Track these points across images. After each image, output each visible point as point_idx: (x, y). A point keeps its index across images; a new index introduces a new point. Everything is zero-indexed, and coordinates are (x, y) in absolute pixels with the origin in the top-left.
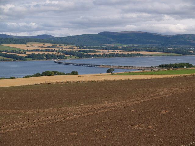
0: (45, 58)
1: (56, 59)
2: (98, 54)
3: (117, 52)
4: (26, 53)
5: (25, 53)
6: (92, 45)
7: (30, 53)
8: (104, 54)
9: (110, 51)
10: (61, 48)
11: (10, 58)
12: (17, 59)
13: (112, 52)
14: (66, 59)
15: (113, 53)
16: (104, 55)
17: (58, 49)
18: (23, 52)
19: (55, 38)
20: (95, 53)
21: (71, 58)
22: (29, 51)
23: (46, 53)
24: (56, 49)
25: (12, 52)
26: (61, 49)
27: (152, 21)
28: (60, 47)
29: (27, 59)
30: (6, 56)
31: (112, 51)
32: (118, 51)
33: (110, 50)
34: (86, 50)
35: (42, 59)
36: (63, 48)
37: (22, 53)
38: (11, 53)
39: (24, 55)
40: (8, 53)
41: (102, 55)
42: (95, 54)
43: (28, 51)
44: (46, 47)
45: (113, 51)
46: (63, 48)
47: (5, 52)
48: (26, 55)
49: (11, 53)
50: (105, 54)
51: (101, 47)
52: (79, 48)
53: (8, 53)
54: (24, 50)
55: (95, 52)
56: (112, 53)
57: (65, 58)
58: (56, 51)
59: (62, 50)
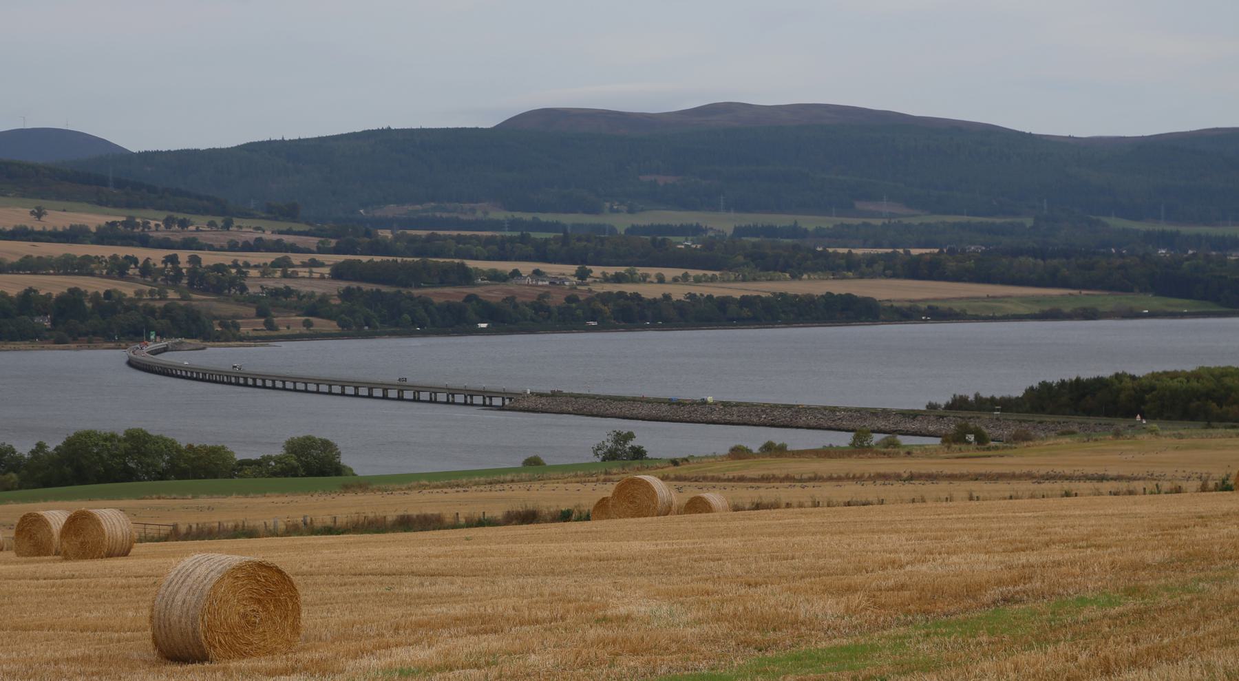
9: (597, 271)
31: (611, 271)
51: (524, 239)
52: (333, 242)
56: (615, 288)
58: (146, 270)
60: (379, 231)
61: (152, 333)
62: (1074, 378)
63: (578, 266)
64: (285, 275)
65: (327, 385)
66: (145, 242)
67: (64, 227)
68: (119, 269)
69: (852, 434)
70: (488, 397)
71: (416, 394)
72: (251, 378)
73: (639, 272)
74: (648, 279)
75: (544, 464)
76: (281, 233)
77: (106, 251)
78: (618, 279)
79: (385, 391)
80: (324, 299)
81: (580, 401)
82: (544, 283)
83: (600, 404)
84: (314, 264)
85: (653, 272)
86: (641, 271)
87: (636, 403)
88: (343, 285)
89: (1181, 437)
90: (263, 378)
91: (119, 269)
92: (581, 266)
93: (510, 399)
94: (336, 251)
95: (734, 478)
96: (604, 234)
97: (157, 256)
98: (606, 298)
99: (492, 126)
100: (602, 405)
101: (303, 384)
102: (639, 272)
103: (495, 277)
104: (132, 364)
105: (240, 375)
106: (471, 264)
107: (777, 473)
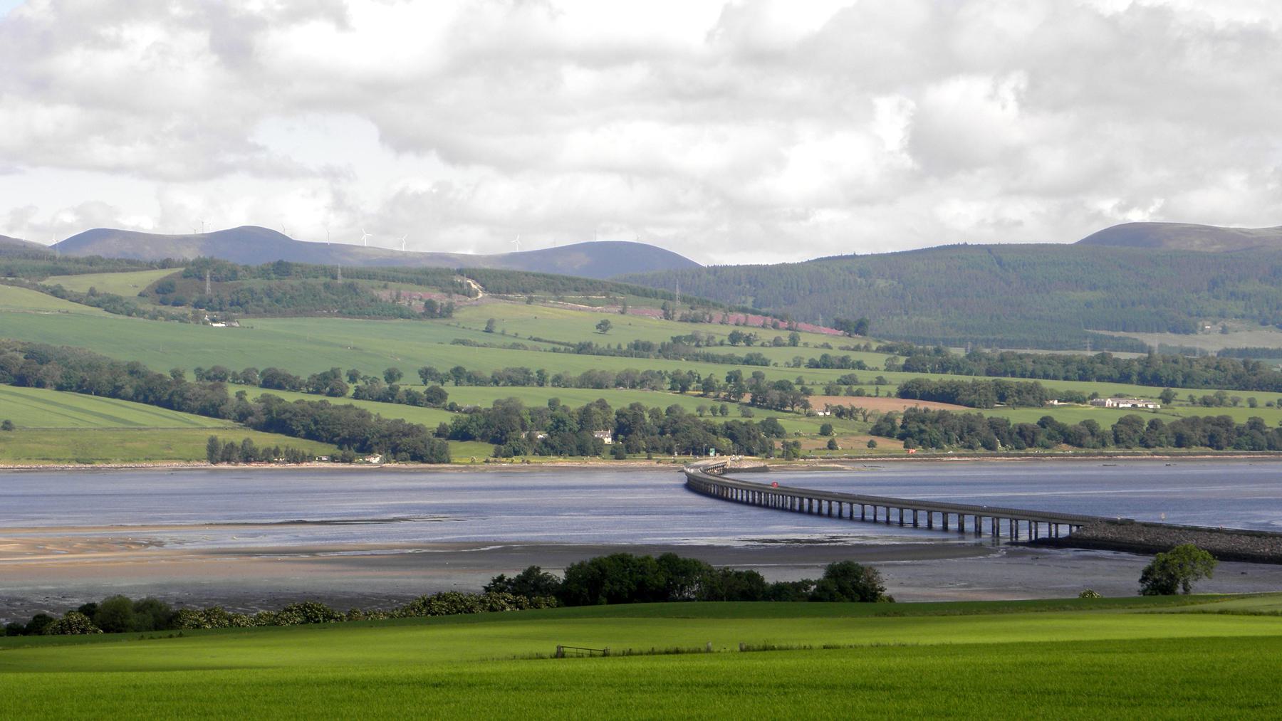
0: (608, 440)
1: (698, 450)
2: (1070, 416)
3: (1253, 404)
4: (443, 396)
5: (435, 399)
6: (1024, 344)
7: (482, 398)
8: (1256, 424)
9: (1182, 393)
10: (747, 362)
11: (310, 435)
12: (365, 448)
13: (1206, 402)
14: (791, 452)
15: (1214, 412)
16: (282, 561)
17: (720, 373)
18: (421, 389)
19: (700, 268)
20: (1044, 412)
21: (831, 446)
22: (475, 380)
23: (619, 399)
24: (704, 370)
25: (326, 383)
26: (747, 372)
27: (904, 615)
28: (741, 351)
29: (455, 447)
30: (276, 423)
31: (1199, 394)
32: (1262, 397)
33: (1184, 385)
34: (968, 379)
35: (583, 451)
36: (765, 363)
37: (413, 400)
38: (318, 392)
39: (431, 419)
40: (289, 397)
41: (1106, 425)
42: (1044, 422)
43: (459, 375)
44: (619, 352)
45: (1210, 393)
46: (765, 363)
47: (266, 384)
48: (447, 418)
49: (316, 398)
50: (1139, 422)
51: (1103, 359)
52: (902, 360)
53: (289, 397)
54: (426, 374)
55: (1041, 399)
56: (1203, 412)
57: (778, 444)
58: (708, 387)
59: (757, 376)
60: (951, 348)
61: (711, 449)
62: (1244, 347)
63: (1163, 388)
64: (850, 393)
65: (898, 508)
66: (708, 359)
67: (179, 260)
68: (680, 384)
69: (1145, 562)
70: (1034, 521)
71: (978, 518)
72: (815, 499)
73: (1229, 396)
74: (1239, 404)
75: (894, 602)
76: (848, 349)
77: (669, 366)
78: (1206, 402)
79: (961, 517)
80: (889, 419)
81: (1153, 530)
82: (1125, 405)
83: (1175, 534)
84: (880, 381)
85: (1245, 395)
86: (1231, 394)
87: (1213, 534)
88: (910, 404)
89: (1131, 608)
90: (819, 498)
91: (680, 384)
92: (1166, 388)
93: (1078, 526)
94: (906, 368)
95: (805, 647)
96: (1195, 355)
97: (720, 373)
98: (1194, 422)
99: (1073, 242)
100: (1176, 536)
101: (860, 506)
102: (1229, 396)
103: (1070, 398)
104: (695, 486)
105: (795, 495)
106: (1046, 384)
107: (841, 642)
